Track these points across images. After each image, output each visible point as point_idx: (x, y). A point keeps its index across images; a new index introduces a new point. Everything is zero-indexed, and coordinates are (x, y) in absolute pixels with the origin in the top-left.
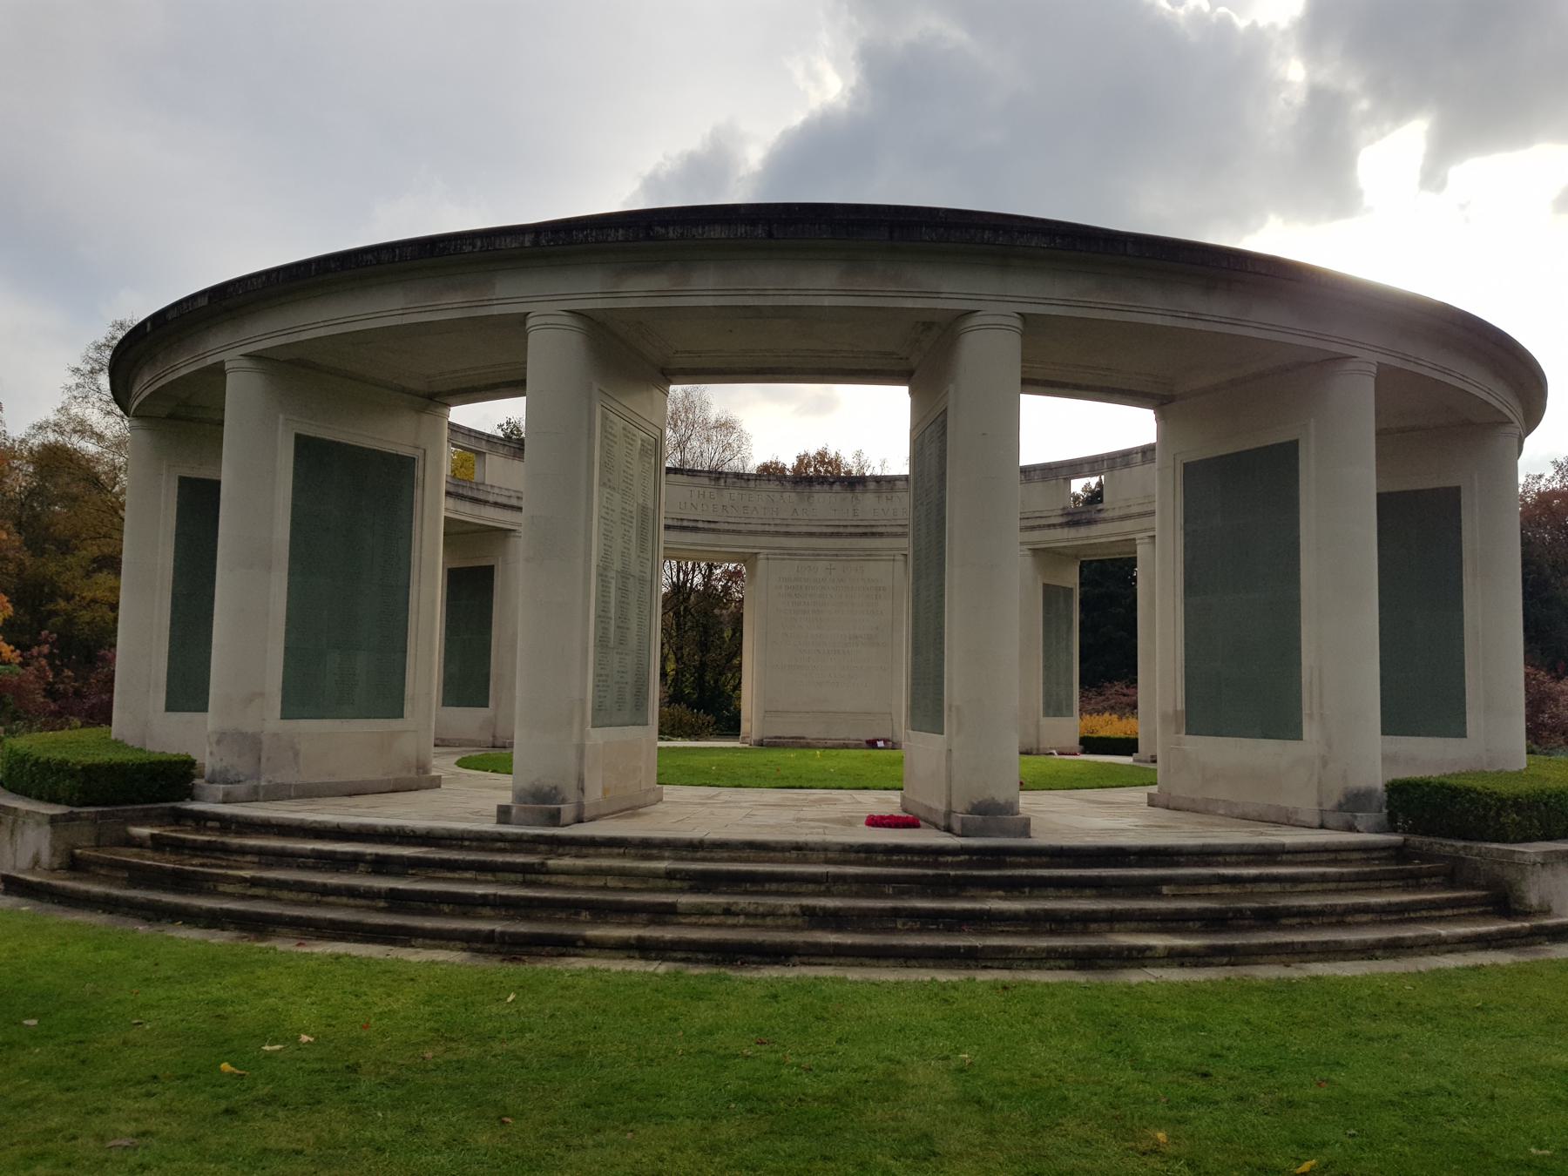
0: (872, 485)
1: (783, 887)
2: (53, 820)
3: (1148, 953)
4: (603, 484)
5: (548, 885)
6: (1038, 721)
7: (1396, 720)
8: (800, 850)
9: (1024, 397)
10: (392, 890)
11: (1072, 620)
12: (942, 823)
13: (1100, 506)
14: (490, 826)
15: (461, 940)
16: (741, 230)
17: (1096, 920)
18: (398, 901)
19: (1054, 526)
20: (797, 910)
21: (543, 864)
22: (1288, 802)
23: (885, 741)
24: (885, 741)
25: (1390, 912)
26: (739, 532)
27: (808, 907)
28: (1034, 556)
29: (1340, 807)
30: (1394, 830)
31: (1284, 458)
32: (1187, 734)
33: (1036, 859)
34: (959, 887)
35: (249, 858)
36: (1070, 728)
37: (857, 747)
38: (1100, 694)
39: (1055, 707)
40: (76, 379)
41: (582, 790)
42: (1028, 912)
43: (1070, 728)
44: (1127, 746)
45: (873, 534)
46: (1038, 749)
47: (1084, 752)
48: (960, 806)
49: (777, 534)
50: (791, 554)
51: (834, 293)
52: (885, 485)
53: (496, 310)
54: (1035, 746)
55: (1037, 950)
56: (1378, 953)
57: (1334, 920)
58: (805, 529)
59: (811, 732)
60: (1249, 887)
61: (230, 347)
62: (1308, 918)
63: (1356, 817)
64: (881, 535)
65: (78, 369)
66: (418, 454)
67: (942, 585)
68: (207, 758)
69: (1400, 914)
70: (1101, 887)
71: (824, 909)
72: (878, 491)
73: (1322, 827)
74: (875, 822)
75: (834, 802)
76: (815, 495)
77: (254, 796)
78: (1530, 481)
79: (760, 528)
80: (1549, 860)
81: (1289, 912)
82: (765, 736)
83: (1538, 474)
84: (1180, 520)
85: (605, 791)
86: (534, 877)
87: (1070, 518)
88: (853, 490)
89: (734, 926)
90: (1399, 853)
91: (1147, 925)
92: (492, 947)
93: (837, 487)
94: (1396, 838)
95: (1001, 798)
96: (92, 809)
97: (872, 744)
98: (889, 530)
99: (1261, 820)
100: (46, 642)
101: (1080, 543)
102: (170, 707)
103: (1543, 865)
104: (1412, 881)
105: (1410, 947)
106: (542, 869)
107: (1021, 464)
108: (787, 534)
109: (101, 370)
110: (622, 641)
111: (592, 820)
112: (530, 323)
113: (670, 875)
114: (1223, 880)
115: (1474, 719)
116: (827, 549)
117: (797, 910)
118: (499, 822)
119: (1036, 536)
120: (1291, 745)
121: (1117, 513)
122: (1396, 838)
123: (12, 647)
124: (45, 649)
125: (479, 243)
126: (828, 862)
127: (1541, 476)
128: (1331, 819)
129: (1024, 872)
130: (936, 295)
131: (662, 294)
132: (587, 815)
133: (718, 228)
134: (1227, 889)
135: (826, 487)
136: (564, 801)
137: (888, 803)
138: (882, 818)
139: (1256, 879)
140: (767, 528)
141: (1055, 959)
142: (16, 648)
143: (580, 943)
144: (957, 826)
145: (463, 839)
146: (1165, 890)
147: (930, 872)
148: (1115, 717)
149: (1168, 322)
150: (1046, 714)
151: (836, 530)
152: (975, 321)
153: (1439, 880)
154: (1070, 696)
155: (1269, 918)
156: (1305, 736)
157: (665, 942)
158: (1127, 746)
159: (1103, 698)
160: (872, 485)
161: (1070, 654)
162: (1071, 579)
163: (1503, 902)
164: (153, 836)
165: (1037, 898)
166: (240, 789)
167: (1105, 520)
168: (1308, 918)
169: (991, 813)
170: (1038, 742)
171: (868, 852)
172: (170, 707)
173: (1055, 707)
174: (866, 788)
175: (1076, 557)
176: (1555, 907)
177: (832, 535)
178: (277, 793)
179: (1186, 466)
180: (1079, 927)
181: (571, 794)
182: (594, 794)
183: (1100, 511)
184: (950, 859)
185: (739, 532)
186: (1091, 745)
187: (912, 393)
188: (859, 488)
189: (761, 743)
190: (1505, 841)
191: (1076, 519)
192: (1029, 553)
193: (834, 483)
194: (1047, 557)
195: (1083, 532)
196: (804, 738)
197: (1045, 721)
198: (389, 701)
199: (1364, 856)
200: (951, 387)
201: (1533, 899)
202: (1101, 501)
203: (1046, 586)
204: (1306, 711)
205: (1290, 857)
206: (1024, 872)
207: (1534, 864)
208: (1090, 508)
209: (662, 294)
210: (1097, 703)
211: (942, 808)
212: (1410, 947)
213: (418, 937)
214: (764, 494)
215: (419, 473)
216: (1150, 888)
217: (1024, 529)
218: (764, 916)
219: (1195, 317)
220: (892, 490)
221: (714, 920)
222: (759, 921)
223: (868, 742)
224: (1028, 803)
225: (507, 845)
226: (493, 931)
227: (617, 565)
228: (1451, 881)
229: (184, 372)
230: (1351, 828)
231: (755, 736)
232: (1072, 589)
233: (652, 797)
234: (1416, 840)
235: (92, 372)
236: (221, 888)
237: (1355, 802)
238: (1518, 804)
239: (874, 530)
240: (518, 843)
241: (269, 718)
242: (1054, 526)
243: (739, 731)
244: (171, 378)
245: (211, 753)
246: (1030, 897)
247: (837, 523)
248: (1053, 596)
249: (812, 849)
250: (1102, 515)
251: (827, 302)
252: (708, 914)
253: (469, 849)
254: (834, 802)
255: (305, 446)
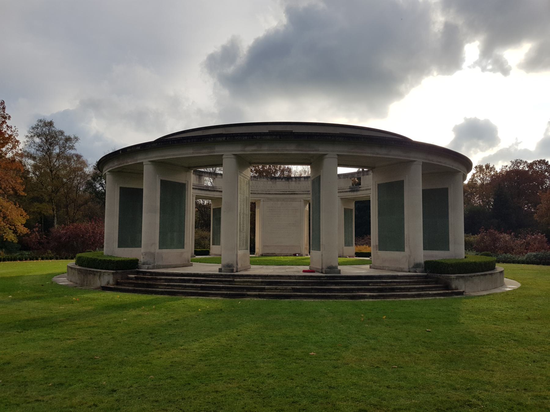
0: (294, 179)
1: (287, 284)
2: (113, 273)
3: (365, 296)
4: (240, 193)
5: (235, 285)
6: (343, 247)
7: (427, 246)
8: (289, 277)
9: (338, 168)
10: (201, 286)
11: (352, 218)
12: (320, 271)
13: (360, 186)
14: (217, 273)
15: (220, 295)
16: (274, 137)
17: (355, 290)
18: (202, 288)
19: (347, 192)
20: (291, 288)
21: (234, 280)
22: (401, 266)
23: (299, 254)
24: (299, 254)
25: (420, 289)
26: (255, 193)
27: (293, 288)
28: (341, 200)
29: (413, 267)
30: (426, 272)
31: (401, 184)
32: (379, 250)
33: (342, 278)
34: (326, 284)
35: (162, 281)
36: (353, 249)
37: (291, 256)
38: (363, 239)
39: (348, 243)
40: (27, 139)
41: (237, 264)
42: (340, 288)
43: (353, 249)
44: (368, 255)
45: (294, 194)
46: (343, 256)
47: (356, 257)
48: (324, 267)
49: (266, 194)
50: (271, 199)
51: (296, 150)
52: (298, 179)
53: (216, 154)
54: (342, 255)
55: (342, 296)
56: (416, 297)
57: (407, 290)
58: (274, 192)
59: (277, 251)
60: (389, 284)
61: (145, 159)
62: (401, 290)
63: (416, 269)
64: (297, 194)
65: (27, 136)
66: (187, 182)
67: (320, 216)
68: (142, 259)
69: (422, 289)
70: (356, 284)
71: (297, 288)
72: (296, 181)
73: (409, 272)
74: (304, 271)
75: (293, 268)
76: (277, 182)
77: (153, 268)
78: (503, 167)
79: (261, 192)
80: (457, 278)
81: (397, 289)
82: (264, 253)
83: (506, 165)
84: (377, 198)
85: (241, 265)
86: (231, 283)
87: (351, 189)
88: (288, 181)
89: (277, 292)
90: (426, 277)
91: (366, 291)
92: (227, 296)
93: (283, 180)
94: (426, 274)
95: (334, 265)
96: (121, 271)
97: (295, 255)
98: (299, 192)
99: (392, 270)
100: (37, 227)
101: (354, 196)
102: (119, 247)
103: (456, 279)
104: (428, 283)
105: (423, 296)
106: (233, 281)
107: (338, 173)
108: (269, 194)
109: (34, 136)
110: (243, 230)
111: (239, 272)
112: (224, 157)
113: (262, 282)
114: (383, 282)
115: (451, 246)
116: (280, 198)
117: (291, 288)
118: (219, 272)
119: (342, 194)
120: (403, 253)
121: (365, 188)
122: (426, 274)
123: (27, 229)
124: (37, 229)
125: (212, 139)
126: (296, 279)
127: (507, 166)
128: (412, 270)
129: (340, 281)
130: (318, 150)
131: (255, 150)
132: (239, 270)
133: (268, 137)
134: (384, 284)
135: (280, 180)
136: (234, 267)
137: (307, 268)
138: (306, 270)
139: (391, 282)
140: (263, 192)
141: (346, 297)
142: (28, 229)
143: (246, 295)
144: (324, 272)
145: (212, 276)
146: (370, 284)
147: (319, 281)
148: (367, 246)
149: (371, 155)
150: (345, 246)
151: (283, 193)
152: (327, 156)
153: (434, 283)
154: (352, 241)
155: (393, 290)
156: (406, 250)
157: (264, 295)
158: (368, 255)
159: (363, 240)
160: (294, 179)
161: (352, 228)
162: (352, 206)
163: (447, 287)
164: (135, 277)
165: (342, 286)
166: (151, 266)
167: (361, 190)
168: (401, 290)
169: (332, 268)
170: (343, 254)
171: (305, 277)
172: (119, 247)
173: (348, 243)
174: (299, 265)
175: (354, 200)
176: (459, 287)
177: (282, 194)
178: (159, 267)
179: (379, 185)
180: (351, 291)
181: (235, 266)
182: (239, 266)
183: (360, 187)
184: (323, 278)
185: (255, 193)
186: (358, 254)
187: (311, 168)
188: (290, 180)
189: (262, 255)
190: (449, 274)
191: (353, 189)
192: (340, 199)
193: (282, 179)
194: (345, 200)
195: (355, 193)
196: (275, 254)
197: (345, 248)
198: (181, 244)
199: (417, 278)
200: (321, 171)
201: (453, 286)
202: (360, 185)
203: (345, 209)
204: (406, 245)
205: (400, 278)
206: (340, 281)
207: (454, 279)
208: (357, 186)
209: (255, 150)
210: (362, 242)
211: (320, 268)
212: (423, 296)
213: (210, 295)
214: (262, 182)
215: (187, 187)
216: (367, 284)
217: (339, 192)
218: (284, 290)
219: (378, 154)
220: (300, 181)
221: (273, 291)
222: (283, 291)
223: (293, 254)
224: (339, 267)
225: (223, 277)
226: (227, 293)
227: (242, 212)
228: (437, 283)
229: (130, 163)
230: (416, 272)
231: (260, 253)
232: (352, 209)
233: (249, 267)
234: (429, 274)
235: (31, 136)
236: (159, 287)
237: (417, 266)
238: (451, 265)
239: (295, 192)
240: (226, 276)
241: (156, 249)
242: (347, 192)
243: (255, 252)
244: (125, 164)
245: (143, 258)
246: (341, 286)
247: (283, 190)
248: (347, 212)
249: (292, 277)
250: (361, 189)
251: (293, 152)
252: (272, 289)
253: (214, 278)
254: (293, 268)
255: (162, 182)
